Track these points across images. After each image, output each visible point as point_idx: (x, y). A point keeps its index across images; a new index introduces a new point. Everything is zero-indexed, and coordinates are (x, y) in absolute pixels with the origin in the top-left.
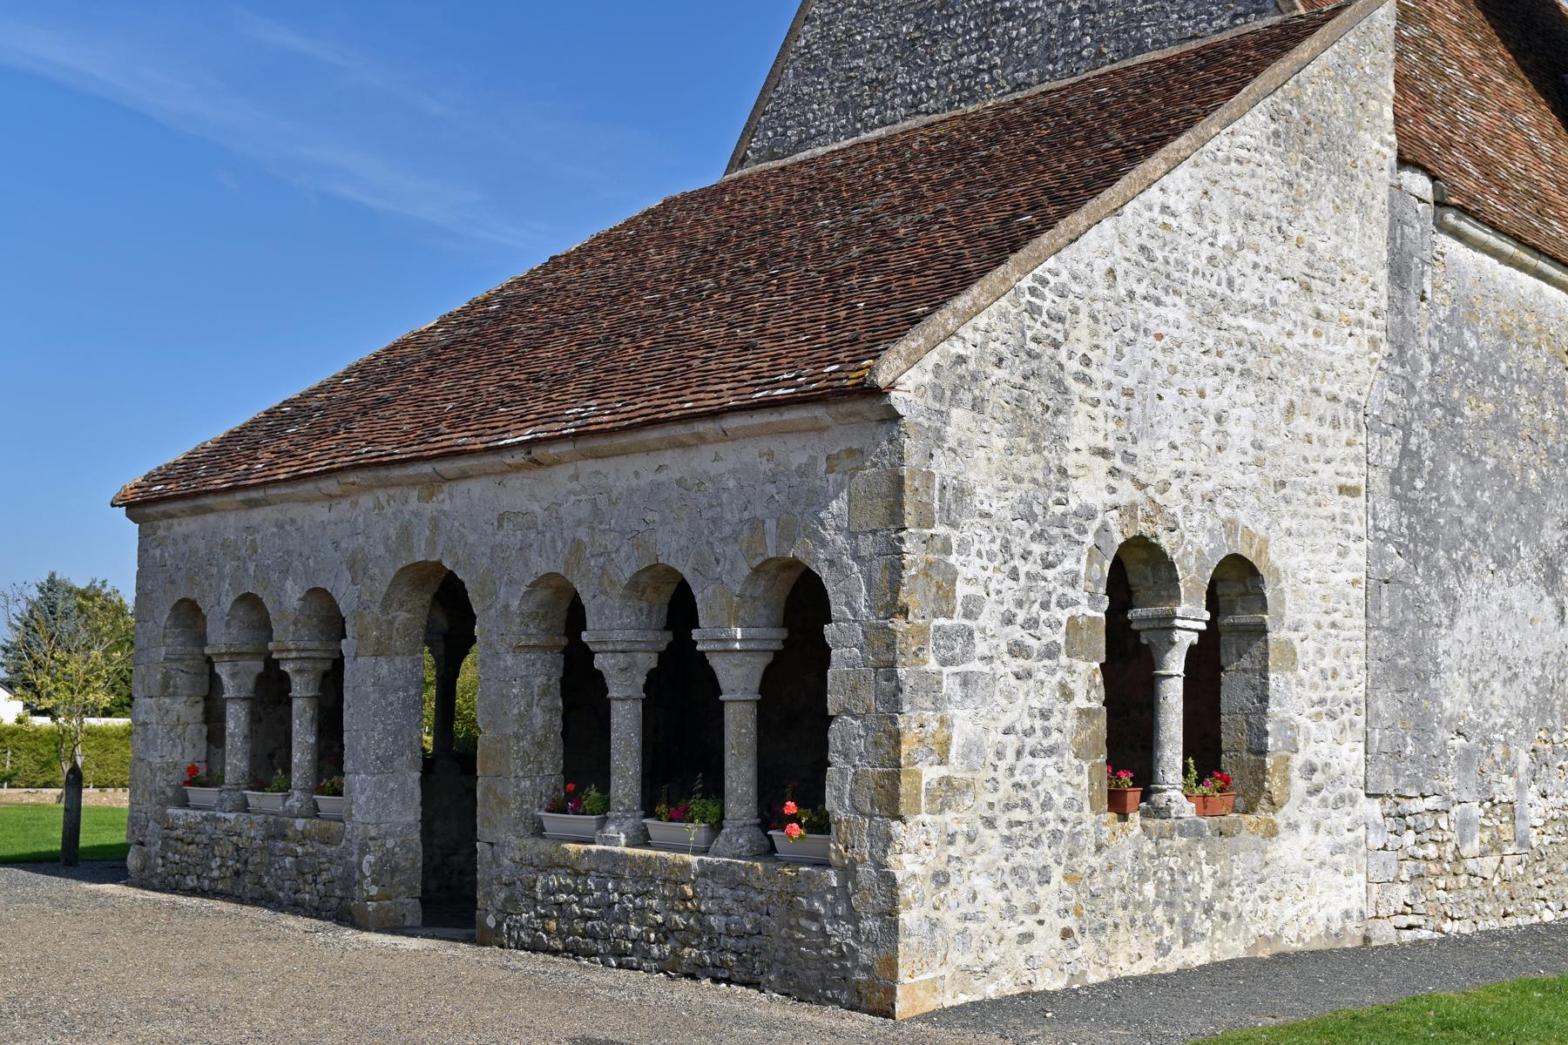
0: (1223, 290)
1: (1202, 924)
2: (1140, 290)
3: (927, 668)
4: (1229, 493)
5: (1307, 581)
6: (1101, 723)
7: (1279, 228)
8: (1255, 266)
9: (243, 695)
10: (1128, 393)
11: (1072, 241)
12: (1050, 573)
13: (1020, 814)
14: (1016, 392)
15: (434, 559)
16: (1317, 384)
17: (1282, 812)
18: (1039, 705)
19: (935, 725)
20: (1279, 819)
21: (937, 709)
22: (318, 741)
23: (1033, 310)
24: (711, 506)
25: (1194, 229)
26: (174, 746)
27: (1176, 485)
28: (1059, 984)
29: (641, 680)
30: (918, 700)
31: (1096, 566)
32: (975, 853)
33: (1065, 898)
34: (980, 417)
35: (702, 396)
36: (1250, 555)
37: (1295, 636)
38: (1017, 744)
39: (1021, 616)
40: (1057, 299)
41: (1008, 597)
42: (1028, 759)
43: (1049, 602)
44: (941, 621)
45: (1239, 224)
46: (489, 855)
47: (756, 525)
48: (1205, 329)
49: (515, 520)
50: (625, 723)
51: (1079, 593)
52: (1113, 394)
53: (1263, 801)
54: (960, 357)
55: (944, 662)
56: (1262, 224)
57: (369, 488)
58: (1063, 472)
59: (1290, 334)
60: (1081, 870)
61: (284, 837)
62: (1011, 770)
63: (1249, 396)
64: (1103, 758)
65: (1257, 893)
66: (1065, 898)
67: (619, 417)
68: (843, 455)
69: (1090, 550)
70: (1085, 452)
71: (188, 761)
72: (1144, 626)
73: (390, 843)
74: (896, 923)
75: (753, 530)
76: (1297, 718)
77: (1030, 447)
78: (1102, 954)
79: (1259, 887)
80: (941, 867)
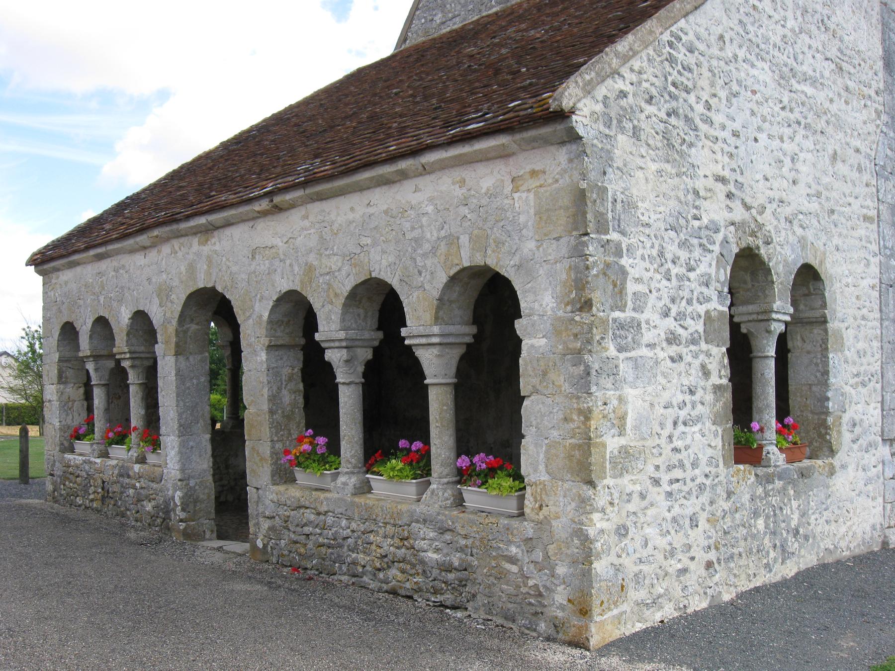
0: (791, 62)
1: (793, 545)
2: (741, 54)
3: (608, 354)
4: (801, 217)
5: (847, 286)
6: (728, 395)
7: (822, 21)
8: (810, 47)
9: (103, 382)
10: (736, 134)
11: (696, 8)
12: (692, 275)
13: (677, 473)
14: (662, 125)
15: (209, 285)
16: (848, 140)
17: (837, 457)
18: (687, 383)
19: (615, 402)
20: (836, 461)
21: (616, 389)
22: (146, 412)
23: (671, 60)
24: (413, 228)
25: (772, 13)
26: (67, 415)
27: (770, 208)
28: (704, 605)
29: (361, 369)
30: (602, 381)
31: (722, 271)
32: (646, 508)
33: (710, 537)
34: (639, 143)
35: (403, 140)
36: (815, 264)
37: (843, 326)
38: (674, 416)
39: (674, 310)
40: (687, 53)
41: (665, 294)
42: (681, 428)
43: (692, 299)
44: (617, 314)
45: (799, 13)
46: (256, 497)
47: (452, 241)
48: (782, 90)
49: (269, 256)
50: (349, 402)
51: (712, 293)
52: (726, 134)
53: (825, 449)
54: (621, 91)
55: (620, 349)
56: (812, 16)
57: (167, 239)
58: (696, 193)
59: (831, 101)
60: (718, 514)
61: (129, 476)
62: (670, 437)
63: (809, 144)
64: (730, 425)
65: (825, 518)
66: (710, 537)
67: (338, 165)
68: (527, 176)
69: (717, 257)
70: (711, 179)
71: (76, 423)
72: (745, 318)
73: (192, 483)
74: (590, 570)
75: (450, 244)
76: (845, 386)
77: (674, 171)
78: (732, 577)
79: (825, 513)
80: (621, 522)
